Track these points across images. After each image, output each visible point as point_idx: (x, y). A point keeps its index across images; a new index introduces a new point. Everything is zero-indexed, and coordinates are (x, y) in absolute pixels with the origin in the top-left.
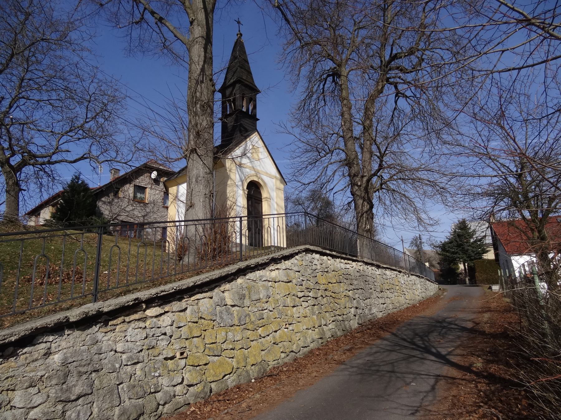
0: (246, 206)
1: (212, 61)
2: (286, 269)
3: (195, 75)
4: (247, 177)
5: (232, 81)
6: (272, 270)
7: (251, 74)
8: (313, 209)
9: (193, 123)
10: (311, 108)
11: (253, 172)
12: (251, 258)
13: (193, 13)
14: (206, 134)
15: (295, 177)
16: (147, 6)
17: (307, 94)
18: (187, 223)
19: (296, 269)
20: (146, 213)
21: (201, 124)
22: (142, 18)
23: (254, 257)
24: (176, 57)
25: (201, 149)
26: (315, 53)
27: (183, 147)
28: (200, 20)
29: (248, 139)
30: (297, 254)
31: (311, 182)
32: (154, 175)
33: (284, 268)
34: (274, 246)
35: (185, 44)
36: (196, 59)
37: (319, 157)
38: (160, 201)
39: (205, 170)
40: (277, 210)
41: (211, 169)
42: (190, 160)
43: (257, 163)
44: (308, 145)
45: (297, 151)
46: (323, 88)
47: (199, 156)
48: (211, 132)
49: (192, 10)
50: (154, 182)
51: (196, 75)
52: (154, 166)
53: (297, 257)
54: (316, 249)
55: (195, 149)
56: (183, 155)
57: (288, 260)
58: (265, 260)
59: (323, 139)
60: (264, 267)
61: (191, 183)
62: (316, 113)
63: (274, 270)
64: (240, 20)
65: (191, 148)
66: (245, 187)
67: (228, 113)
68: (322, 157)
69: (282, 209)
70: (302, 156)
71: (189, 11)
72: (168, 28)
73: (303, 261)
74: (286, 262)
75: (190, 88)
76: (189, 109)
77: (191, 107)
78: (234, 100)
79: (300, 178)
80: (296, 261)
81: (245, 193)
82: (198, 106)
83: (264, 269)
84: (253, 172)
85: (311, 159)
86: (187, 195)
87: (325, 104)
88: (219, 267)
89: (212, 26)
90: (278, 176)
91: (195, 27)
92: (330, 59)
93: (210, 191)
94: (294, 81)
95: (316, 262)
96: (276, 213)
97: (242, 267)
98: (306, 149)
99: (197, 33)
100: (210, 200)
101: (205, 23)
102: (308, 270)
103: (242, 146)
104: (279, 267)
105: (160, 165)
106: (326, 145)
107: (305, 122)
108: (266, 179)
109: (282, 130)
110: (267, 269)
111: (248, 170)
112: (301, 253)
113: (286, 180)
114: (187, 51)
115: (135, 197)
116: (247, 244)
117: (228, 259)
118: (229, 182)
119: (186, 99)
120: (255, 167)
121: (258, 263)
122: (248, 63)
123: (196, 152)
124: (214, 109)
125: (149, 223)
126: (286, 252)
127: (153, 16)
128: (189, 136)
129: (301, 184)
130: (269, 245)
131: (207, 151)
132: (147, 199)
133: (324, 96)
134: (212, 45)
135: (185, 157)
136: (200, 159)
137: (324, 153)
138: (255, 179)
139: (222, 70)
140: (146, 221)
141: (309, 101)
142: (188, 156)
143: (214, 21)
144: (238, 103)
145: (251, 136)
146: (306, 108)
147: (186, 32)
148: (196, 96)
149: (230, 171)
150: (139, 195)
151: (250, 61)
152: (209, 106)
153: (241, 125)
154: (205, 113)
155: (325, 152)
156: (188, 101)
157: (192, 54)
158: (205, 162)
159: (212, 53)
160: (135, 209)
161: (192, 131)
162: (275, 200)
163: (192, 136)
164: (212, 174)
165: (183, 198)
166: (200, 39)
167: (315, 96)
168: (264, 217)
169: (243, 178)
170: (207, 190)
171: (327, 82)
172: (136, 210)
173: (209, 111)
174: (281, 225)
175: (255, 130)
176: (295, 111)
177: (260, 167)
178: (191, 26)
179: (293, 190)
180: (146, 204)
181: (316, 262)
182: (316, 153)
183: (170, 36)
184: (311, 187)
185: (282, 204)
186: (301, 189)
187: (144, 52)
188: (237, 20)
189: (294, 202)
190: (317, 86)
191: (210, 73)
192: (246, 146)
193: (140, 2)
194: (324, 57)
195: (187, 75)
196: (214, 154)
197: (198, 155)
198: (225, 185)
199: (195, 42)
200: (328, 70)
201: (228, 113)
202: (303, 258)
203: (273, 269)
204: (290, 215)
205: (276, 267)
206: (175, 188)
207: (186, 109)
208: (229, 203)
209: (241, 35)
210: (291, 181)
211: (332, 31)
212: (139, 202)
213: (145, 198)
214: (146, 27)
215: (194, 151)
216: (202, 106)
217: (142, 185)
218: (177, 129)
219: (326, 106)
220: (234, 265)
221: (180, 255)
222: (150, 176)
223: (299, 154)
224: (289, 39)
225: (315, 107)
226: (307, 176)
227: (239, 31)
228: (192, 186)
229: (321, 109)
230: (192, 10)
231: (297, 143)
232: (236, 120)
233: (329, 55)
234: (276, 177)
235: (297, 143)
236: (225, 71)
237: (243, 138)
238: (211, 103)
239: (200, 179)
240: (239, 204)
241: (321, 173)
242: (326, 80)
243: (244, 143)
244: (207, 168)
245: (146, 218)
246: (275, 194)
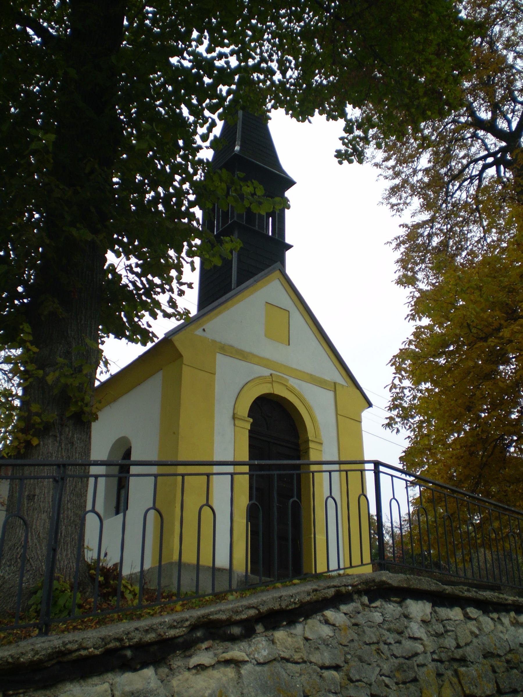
53: (329, 614)
80: (326, 631)
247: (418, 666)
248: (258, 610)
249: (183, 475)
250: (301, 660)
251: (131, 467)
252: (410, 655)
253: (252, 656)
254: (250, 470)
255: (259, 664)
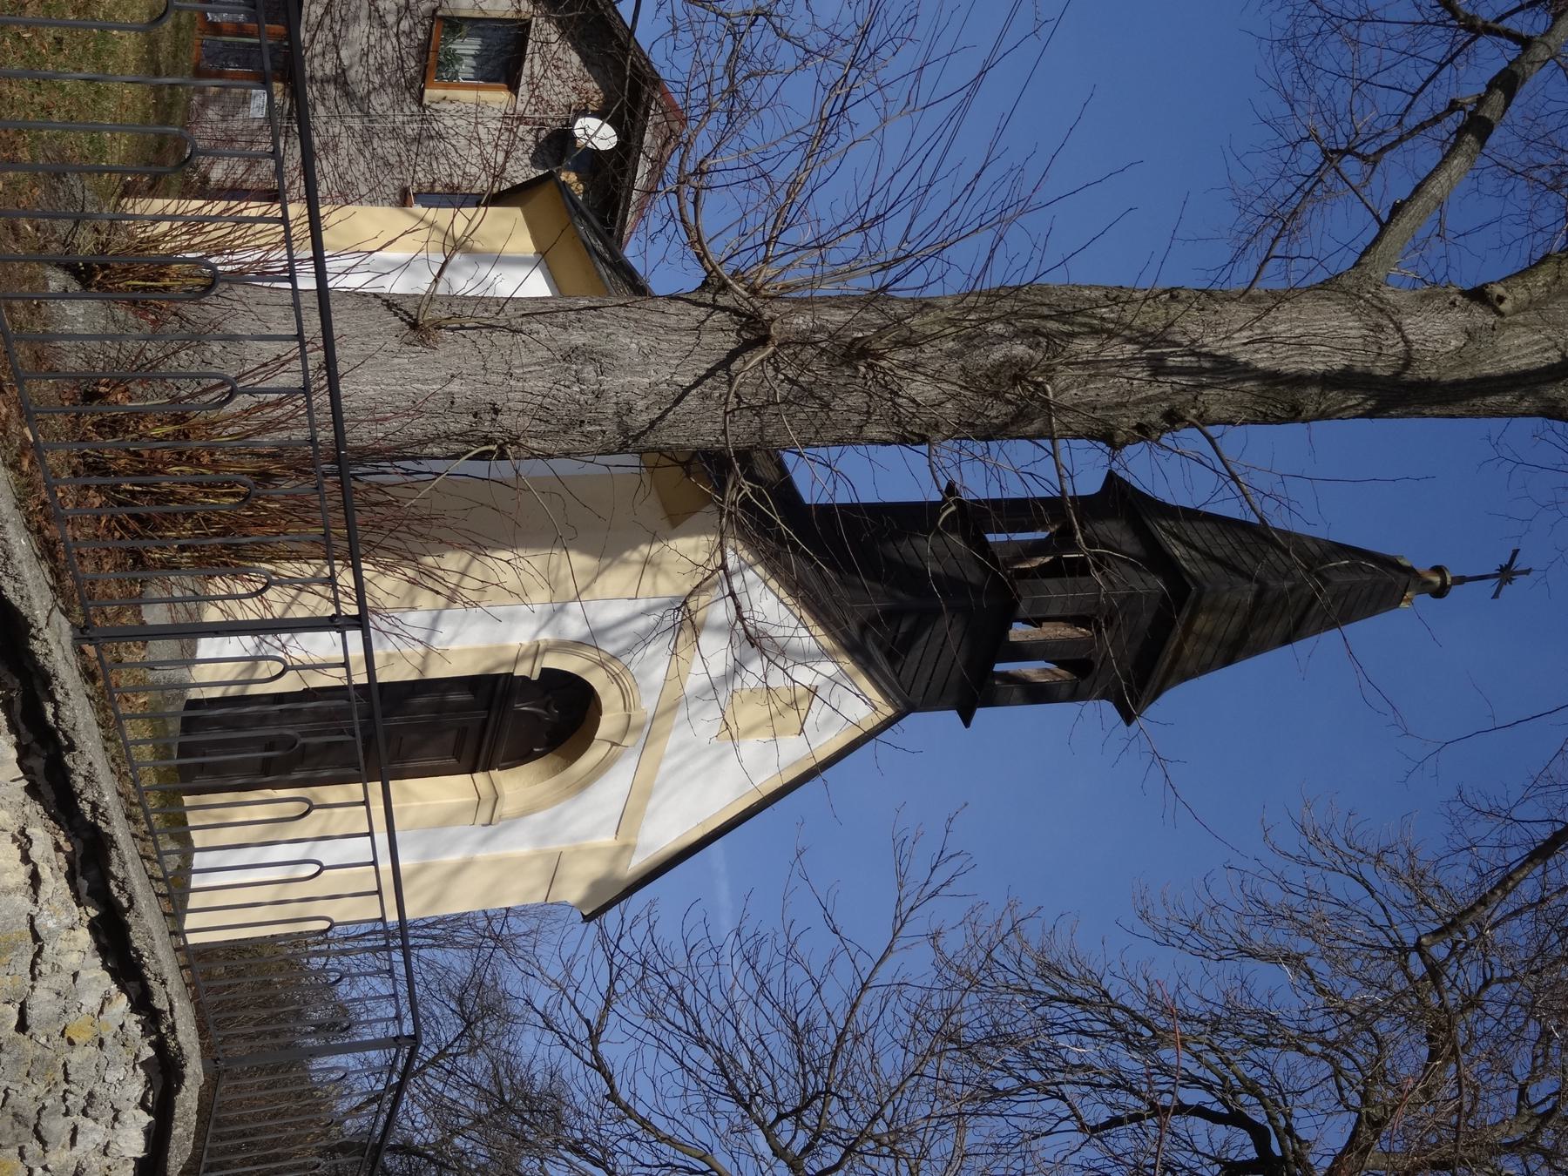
0: (437, 671)
1: (1279, 421)
2: (36, 937)
3: (1192, 327)
4: (615, 667)
5: (1178, 551)
6: (23, 841)
7: (1229, 661)
8: (439, 1107)
9: (915, 322)
10: (1062, 1041)
11: (647, 705)
12: (105, 702)
13: (1532, 304)
14: (857, 400)
15: (636, 970)
16: (1541, 52)
17: (1138, 1007)
18: (310, 304)
19: (43, 1003)
20: (361, 90)
21: (913, 367)
22: (1476, 29)
23: (110, 725)
24: (1286, 221)
25: (770, 372)
26: (1379, 1043)
27: (769, 271)
28: (1502, 344)
29: (847, 664)
30: (142, 1002)
31: (609, 1079)
32: (598, 134)
33: (47, 923)
34: (186, 870)
35: (1357, 264)
36: (1283, 324)
37: (772, 1116)
38: (442, 170)
39: (641, 405)
40: (421, 870)
41: (651, 440)
42: (700, 313)
43: (707, 722)
44: (840, 1038)
45: (797, 975)
46: (1182, 1109)
47: (725, 364)
48: (873, 431)
49: (1551, 296)
50: (549, 139)
51: (1195, 330)
52: (647, 138)
53: (122, 1003)
54: (178, 1131)
55: (763, 340)
56: (725, 271)
57: (102, 950)
58: (89, 794)
59: (880, 1128)
60: (45, 788)
61: (561, 318)
62: (1035, 1076)
63: (26, 859)
64: (1520, 581)
65: (767, 313)
66: (552, 662)
67: (990, 538)
68: (768, 1131)
69: (435, 901)
70: (766, 1006)
71: (1542, 277)
72: (1438, 168)
73: (92, 1050)
74: (84, 937)
75: (1115, 297)
76: (995, 295)
77: (1007, 305)
78: (1079, 568)
79: (630, 1010)
80: (91, 1001)
81: (516, 661)
82: (1020, 350)
83: (33, 791)
84: (647, 705)
85: (757, 1064)
86: (479, 300)
87: (1094, 1129)
88: (33, 505)
89: (1474, 414)
90: (636, 864)
91: (1458, 316)
92: (1354, 1134)
93: (515, 441)
94: (1208, 925)
95: (93, 1133)
96: (403, 863)
97: (36, 646)
98: (810, 1027)
99: (1429, 329)
100: (463, 437)
101: (1488, 370)
102: (38, 1089)
103: (804, 634)
104: (46, 890)
105: (659, 164)
106: (849, 1150)
107: (973, 1017)
108: (613, 788)
109: (918, 871)
110: (34, 809)
111: (659, 674)
112: (146, 1032)
113: (612, 916)
114: (1321, 275)
115: (455, 25)
116: (194, 694)
117: (89, 566)
118: (580, 561)
119: (1053, 280)
120: (681, 714)
121: (71, 747)
122: (1287, 640)
123: (746, 347)
124: (1009, 445)
125: (301, 113)
126: (160, 961)
127: (1491, 87)
128: (839, 302)
129: (592, 1014)
130: (198, 838)
131: (757, 410)
132: (451, 94)
133: (1137, 1118)
134: (1369, 414)
135: (714, 284)
136: (711, 373)
137: (797, 1148)
138: (608, 724)
139: (1234, 478)
140: (312, 92)
141: (1098, 1026)
142: (722, 300)
143: (1497, 424)
144: (1056, 592)
145: (864, 684)
146: (1056, 1012)
147: (1423, 271)
148: (1072, 335)
149: (647, 562)
150: (467, 47)
151: (1301, 646)
152: (1021, 416)
153: (926, 617)
154: (981, 392)
155: (808, 1149)
156: (1043, 289)
157: (1307, 303)
158: (691, 401)
159: (1323, 416)
160: (384, 25)
161: (873, 317)
162: (482, 854)
163: (839, 317)
164: (623, 449)
165: (463, 282)
166: (1393, 346)
167: (1130, 1062)
168: (376, 787)
169: (610, 649)
170: (524, 421)
171: (1221, 1132)
172: (377, 32)
173: (997, 412)
174: (330, 882)
175: (907, 700)
176: (1034, 945)
177: (681, 747)
178: (1463, 293)
179: (555, 971)
180: (414, 89)
181: (93, 1133)
182: (789, 1092)
183: (1393, 181)
184: (582, 1087)
185: (463, 900)
186: (566, 1017)
187: (1291, 43)
188: (1521, 563)
189: (477, 983)
190: (1194, 1069)
191: (1215, 411)
192: (804, 658)
193: (1557, 17)
194: (1365, 1097)
195: (1190, 280)
196: (744, 456)
197: (733, 355)
198: (560, 536)
199: (1376, 317)
200: (1289, 1130)
201: (990, 538)
202: (112, 1050)
203: (36, 852)
204: (401, 970)
205: (45, 872)
206: (524, 244)
207: (993, 281)
208: (453, 561)
209: (1440, 592)
210: (607, 943)
211: (1517, 1135)
212: (424, 49)
213: (452, 82)
214: (1431, 54)
215: (754, 332)
216: (1018, 373)
217: (532, 66)
218: (874, 233)
219: (1081, 1137)
220: (49, 595)
221: (104, 267)
222: (585, 113)
223: (775, 989)
224: (1445, 877)
225: (1067, 1067)
226: (649, 1052)
227: (1460, 580)
228: (542, 330)
229: (1063, 1110)
230: (1551, 296)
231: (843, 968)
232: (953, 585)
233: (1377, 1125)
234: (627, 849)
235: (843, 968)
236: (1231, 508)
237: (854, 630)
238: (1037, 425)
239: (589, 372)
240: (445, 631)
241: (669, 1140)
242: (1236, 1119)
243: (826, 641)
244: (654, 415)
245: (331, 90)
246: (523, 850)
247: (21, 1149)
248: (128, 910)
249: (366, 803)
250: (37, 972)
251: (359, 632)
252: (43, 1133)
253: (45, 907)
254: (357, 687)
255: (32, 919)
